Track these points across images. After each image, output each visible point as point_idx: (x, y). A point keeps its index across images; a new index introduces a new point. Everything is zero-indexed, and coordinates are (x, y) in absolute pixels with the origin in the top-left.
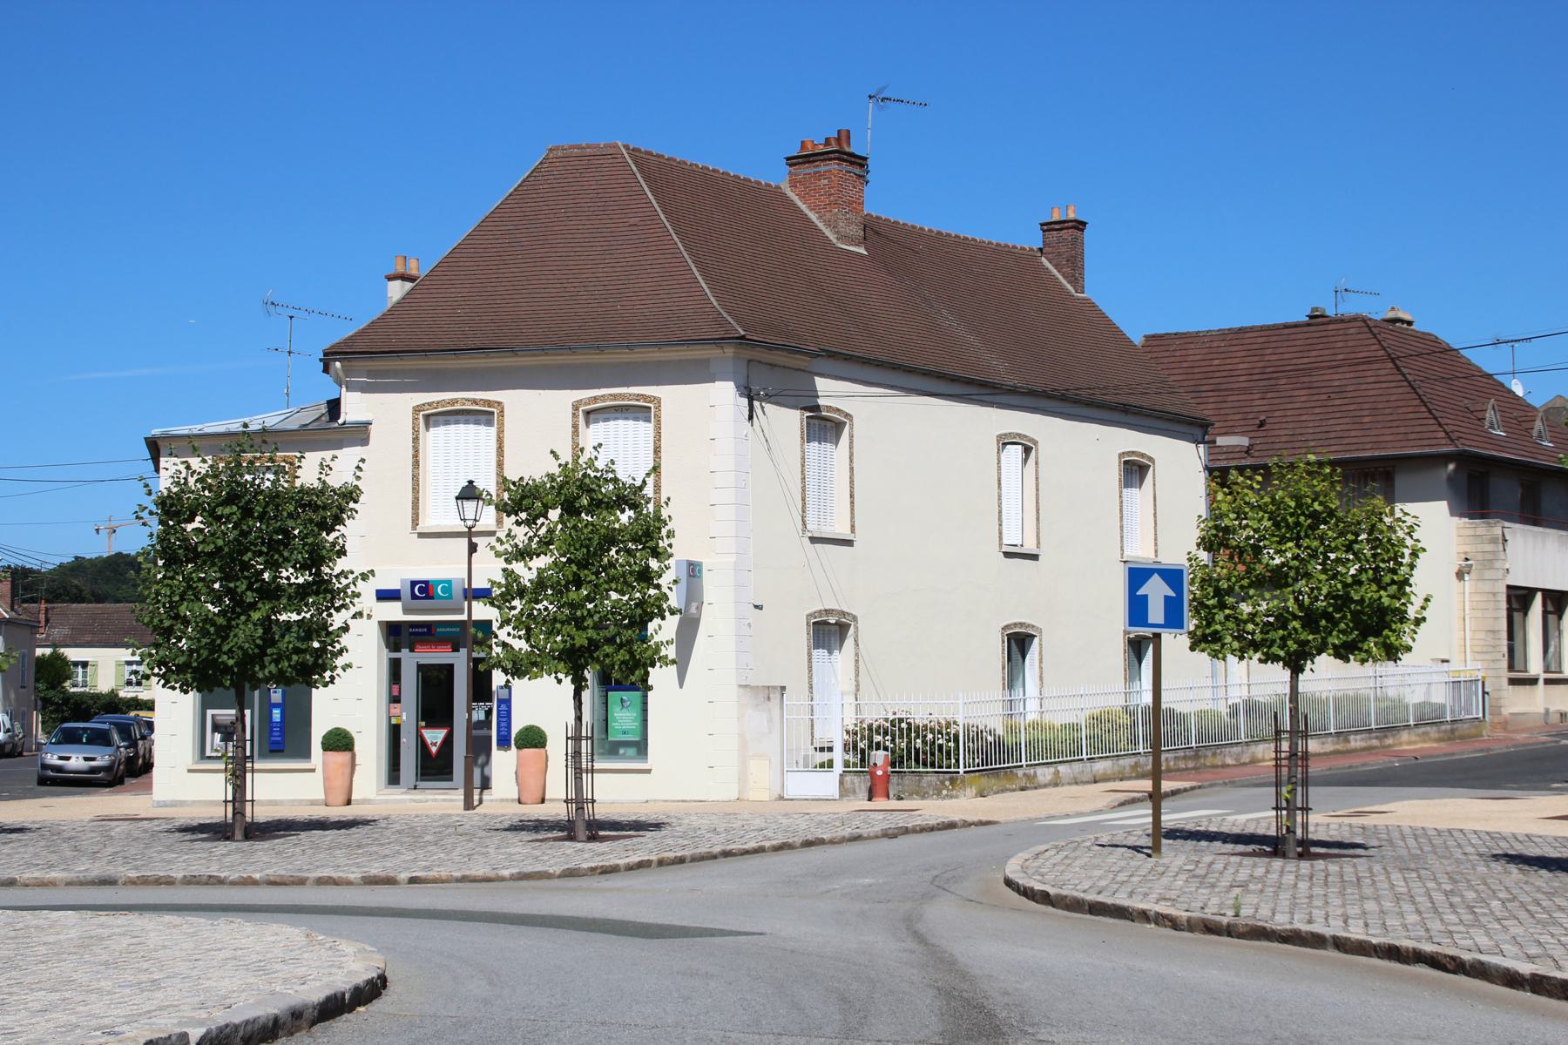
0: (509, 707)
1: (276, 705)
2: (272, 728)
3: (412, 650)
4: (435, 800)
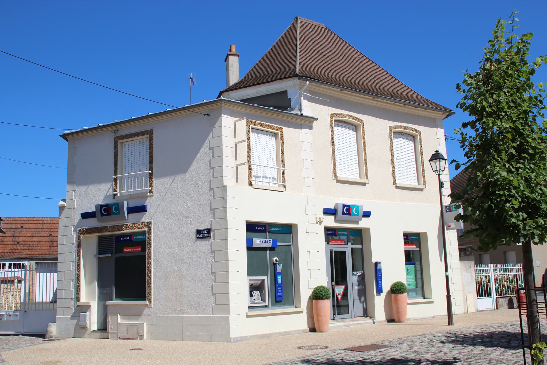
1: (280, 274)
4: (354, 324)
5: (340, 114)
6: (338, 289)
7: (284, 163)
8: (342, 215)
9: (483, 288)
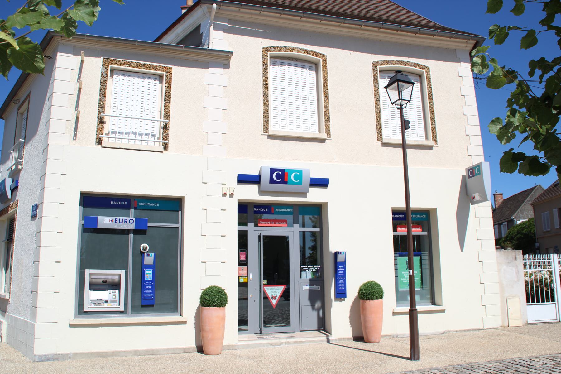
0: (345, 268)
1: (149, 267)
2: (145, 286)
3: (256, 225)
4: (288, 343)
5: (281, 48)
6: (271, 290)
7: (169, 113)
8: (270, 183)
9: (545, 289)
